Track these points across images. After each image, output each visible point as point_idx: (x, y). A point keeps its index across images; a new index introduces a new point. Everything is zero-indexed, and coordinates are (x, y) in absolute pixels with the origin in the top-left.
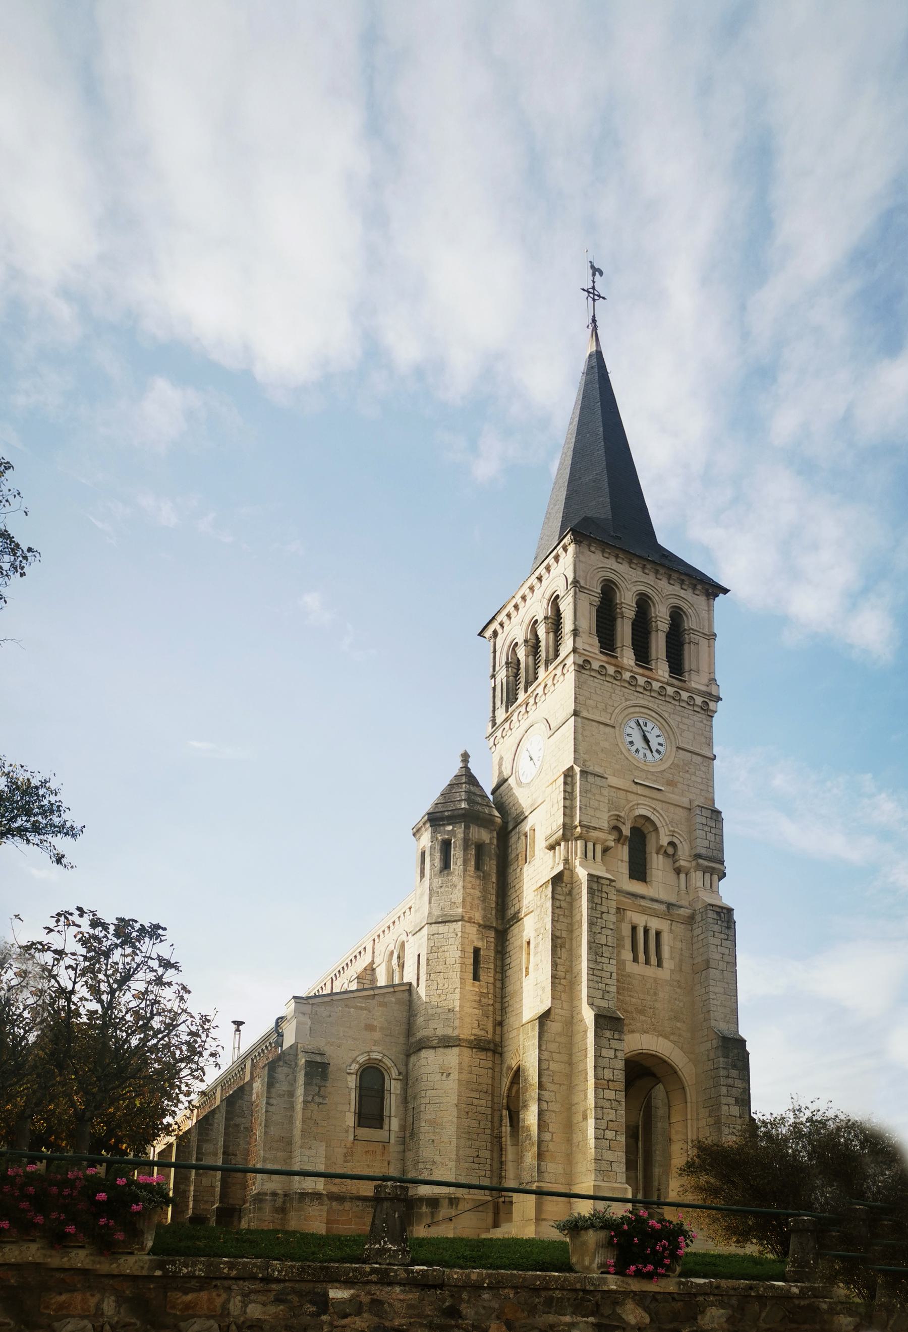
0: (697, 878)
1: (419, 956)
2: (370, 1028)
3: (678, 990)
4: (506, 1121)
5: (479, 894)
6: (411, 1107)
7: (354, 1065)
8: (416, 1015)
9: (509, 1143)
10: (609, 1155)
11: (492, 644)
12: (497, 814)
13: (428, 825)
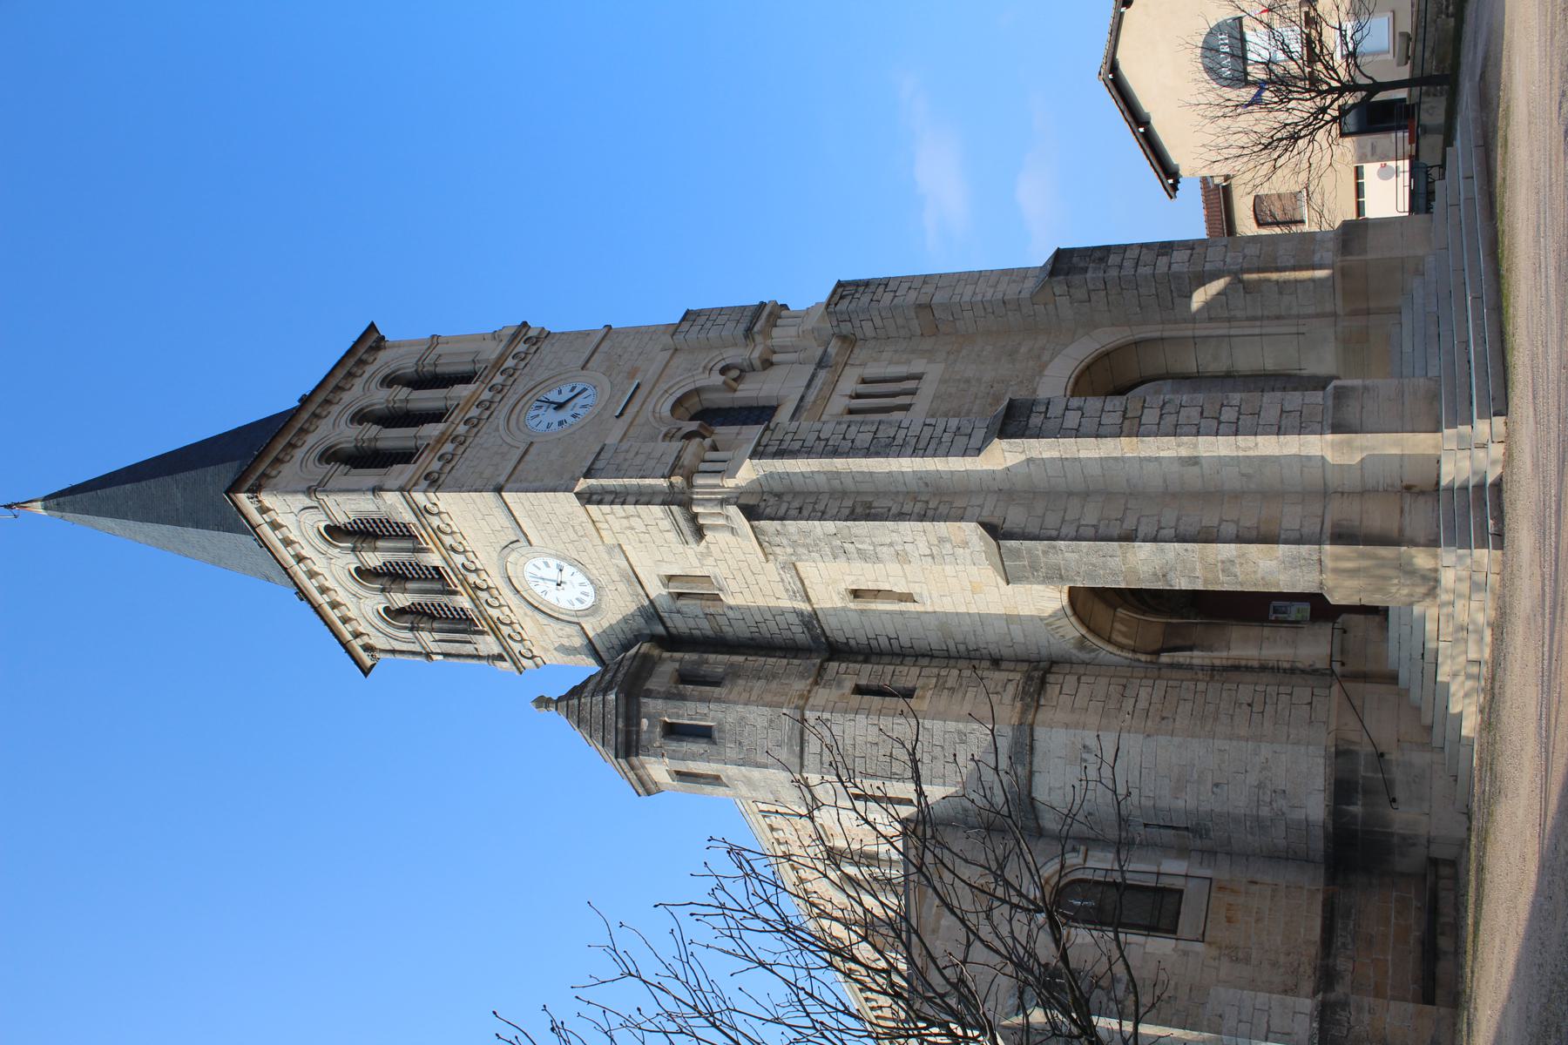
0: (781, 335)
3: (964, 352)
5: (763, 682)
9: (1224, 654)
10: (1271, 415)
13: (634, 760)
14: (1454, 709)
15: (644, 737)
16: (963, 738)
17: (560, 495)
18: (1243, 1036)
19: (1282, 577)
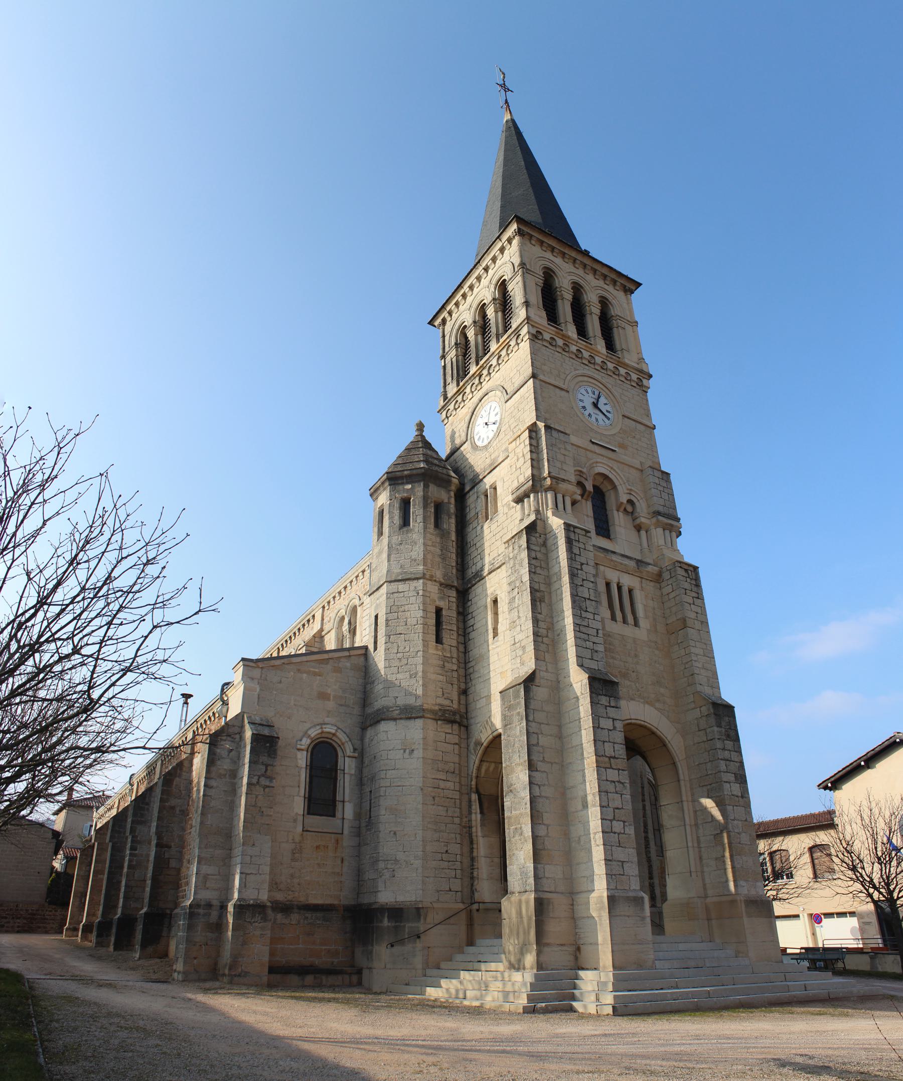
0: (658, 535)
1: (376, 617)
2: (323, 696)
3: (657, 652)
5: (438, 551)
6: (368, 790)
7: (304, 740)
8: (373, 682)
9: (480, 834)
10: (620, 854)
11: (441, 330)
12: (453, 474)
13: (387, 484)
14: (444, 982)
15: (401, 487)
16: (413, 676)
17: (534, 413)
18: (242, 859)
19: (515, 867)
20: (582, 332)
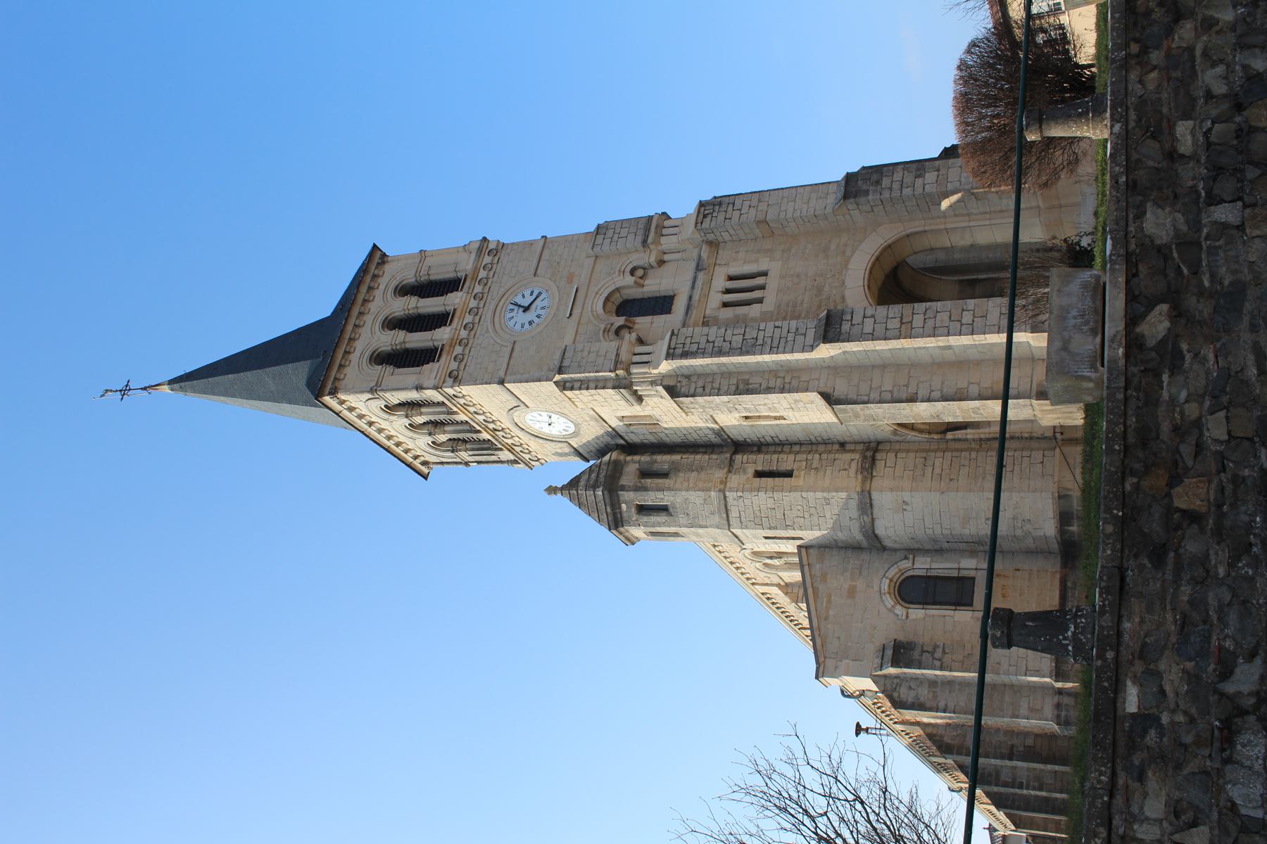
0: (667, 242)
2: (852, 592)
3: (793, 251)
4: (959, 434)
5: (695, 474)
11: (434, 466)
12: (606, 458)
13: (621, 529)
15: (625, 515)
20: (441, 320)
